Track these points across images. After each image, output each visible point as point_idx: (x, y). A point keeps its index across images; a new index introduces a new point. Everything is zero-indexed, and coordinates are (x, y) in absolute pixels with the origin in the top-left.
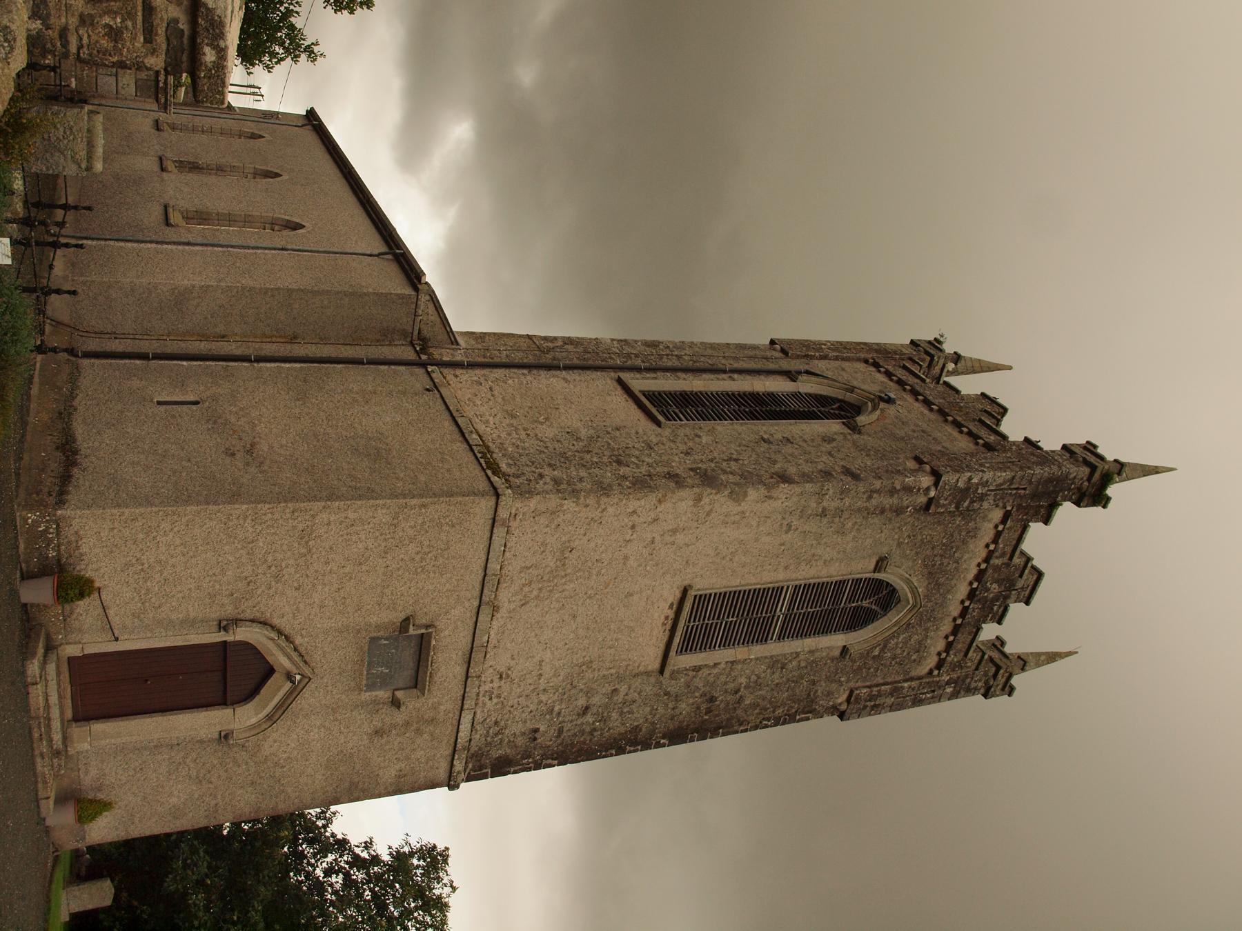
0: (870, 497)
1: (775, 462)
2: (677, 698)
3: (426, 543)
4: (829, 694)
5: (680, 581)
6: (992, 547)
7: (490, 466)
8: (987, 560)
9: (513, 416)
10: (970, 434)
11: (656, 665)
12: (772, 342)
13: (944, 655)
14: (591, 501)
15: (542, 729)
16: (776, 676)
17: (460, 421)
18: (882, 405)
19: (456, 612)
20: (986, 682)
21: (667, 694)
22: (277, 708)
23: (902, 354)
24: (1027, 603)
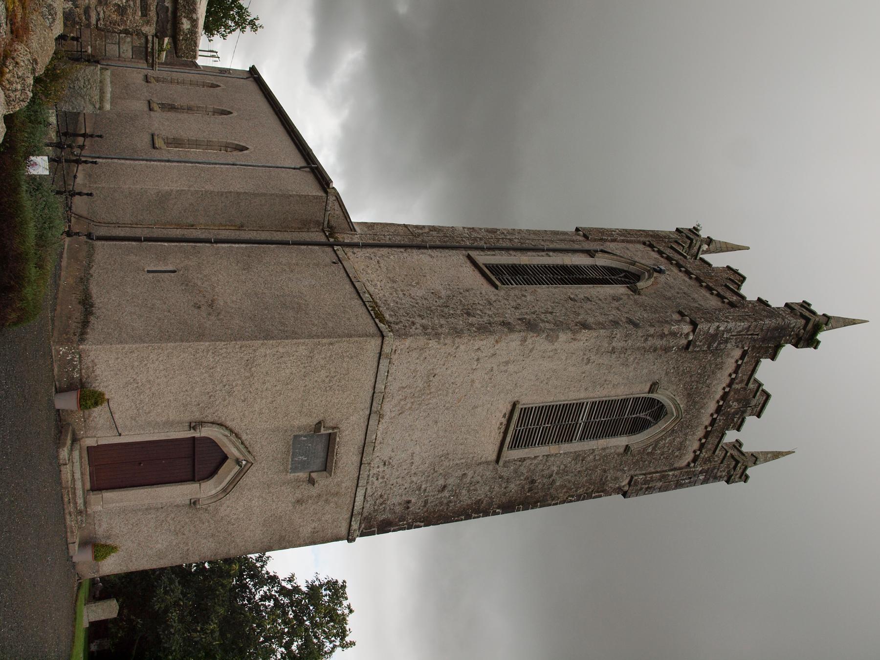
0: (646, 340)
1: (579, 314)
3: (333, 370)
4: (616, 479)
5: (511, 398)
6: (733, 376)
7: (377, 316)
8: (730, 385)
9: (394, 282)
10: (718, 295)
12: (577, 230)
13: (698, 453)
15: (413, 500)
16: (579, 465)
17: (357, 284)
18: (655, 274)
19: (353, 418)
20: (728, 472)
22: (230, 483)
23: (669, 238)
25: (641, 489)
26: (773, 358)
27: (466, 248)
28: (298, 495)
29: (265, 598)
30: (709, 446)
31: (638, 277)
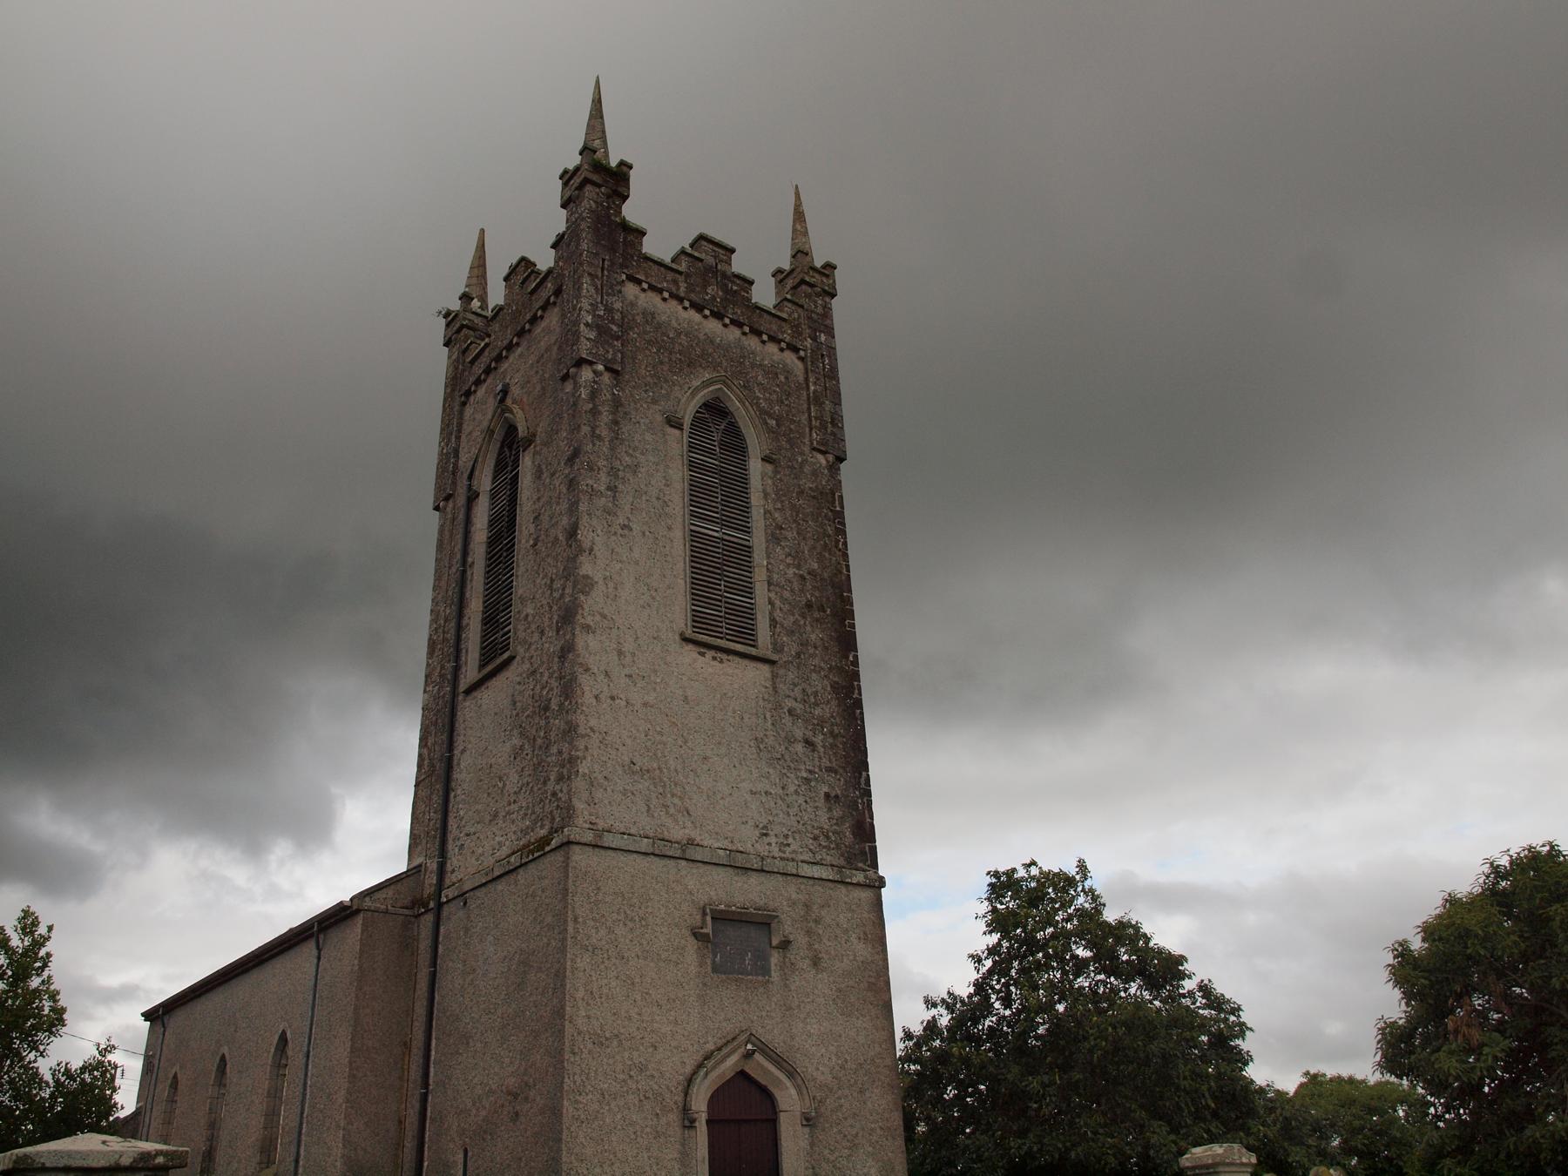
0: (599, 438)
1: (556, 539)
2: (804, 644)
3: (615, 916)
4: (815, 473)
5: (675, 644)
6: (666, 295)
7: (539, 849)
8: (681, 300)
9: (496, 816)
10: (544, 308)
11: (766, 668)
12: (437, 508)
13: (783, 345)
14: (581, 744)
15: (826, 789)
16: (789, 535)
17: (497, 873)
18: (509, 401)
19: (691, 884)
20: (818, 295)
21: (798, 655)
22: (781, 1068)
23: (457, 360)
24: (732, 251)
25: (833, 434)
26: (642, 233)
27: (454, 694)
28: (806, 964)
29: (1007, 1003)
30: (774, 327)
31: (511, 429)
